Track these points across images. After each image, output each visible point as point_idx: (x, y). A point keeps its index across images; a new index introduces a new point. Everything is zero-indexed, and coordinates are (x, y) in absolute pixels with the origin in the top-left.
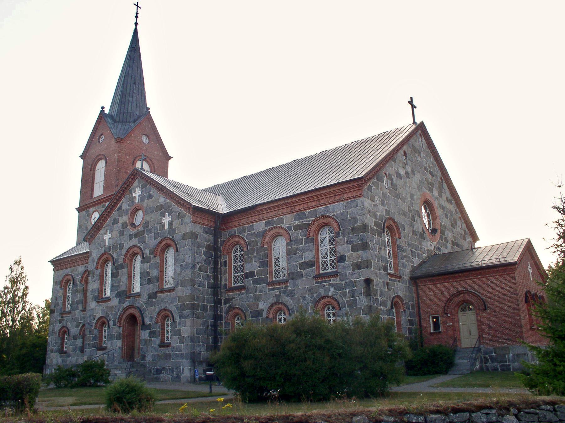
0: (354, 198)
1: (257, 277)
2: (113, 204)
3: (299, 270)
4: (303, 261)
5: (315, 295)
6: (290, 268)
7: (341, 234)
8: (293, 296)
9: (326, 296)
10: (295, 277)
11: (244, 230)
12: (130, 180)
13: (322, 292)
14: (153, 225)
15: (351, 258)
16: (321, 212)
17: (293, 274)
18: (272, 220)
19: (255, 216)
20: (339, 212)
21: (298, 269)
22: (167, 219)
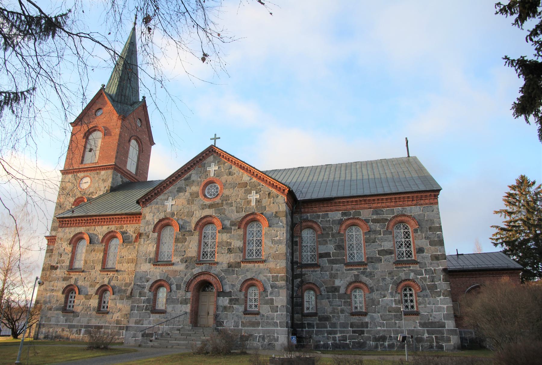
0: (430, 204)
1: (332, 258)
2: (180, 173)
3: (378, 256)
4: (382, 248)
5: (395, 278)
6: (369, 253)
7: (419, 231)
8: (373, 277)
9: (406, 280)
10: (373, 261)
11: (318, 217)
12: (204, 155)
13: (403, 276)
14: (235, 199)
15: (429, 250)
16: (398, 212)
17: (372, 258)
18: (348, 212)
19: (331, 206)
20: (417, 213)
21: (377, 255)
22: (254, 197)
